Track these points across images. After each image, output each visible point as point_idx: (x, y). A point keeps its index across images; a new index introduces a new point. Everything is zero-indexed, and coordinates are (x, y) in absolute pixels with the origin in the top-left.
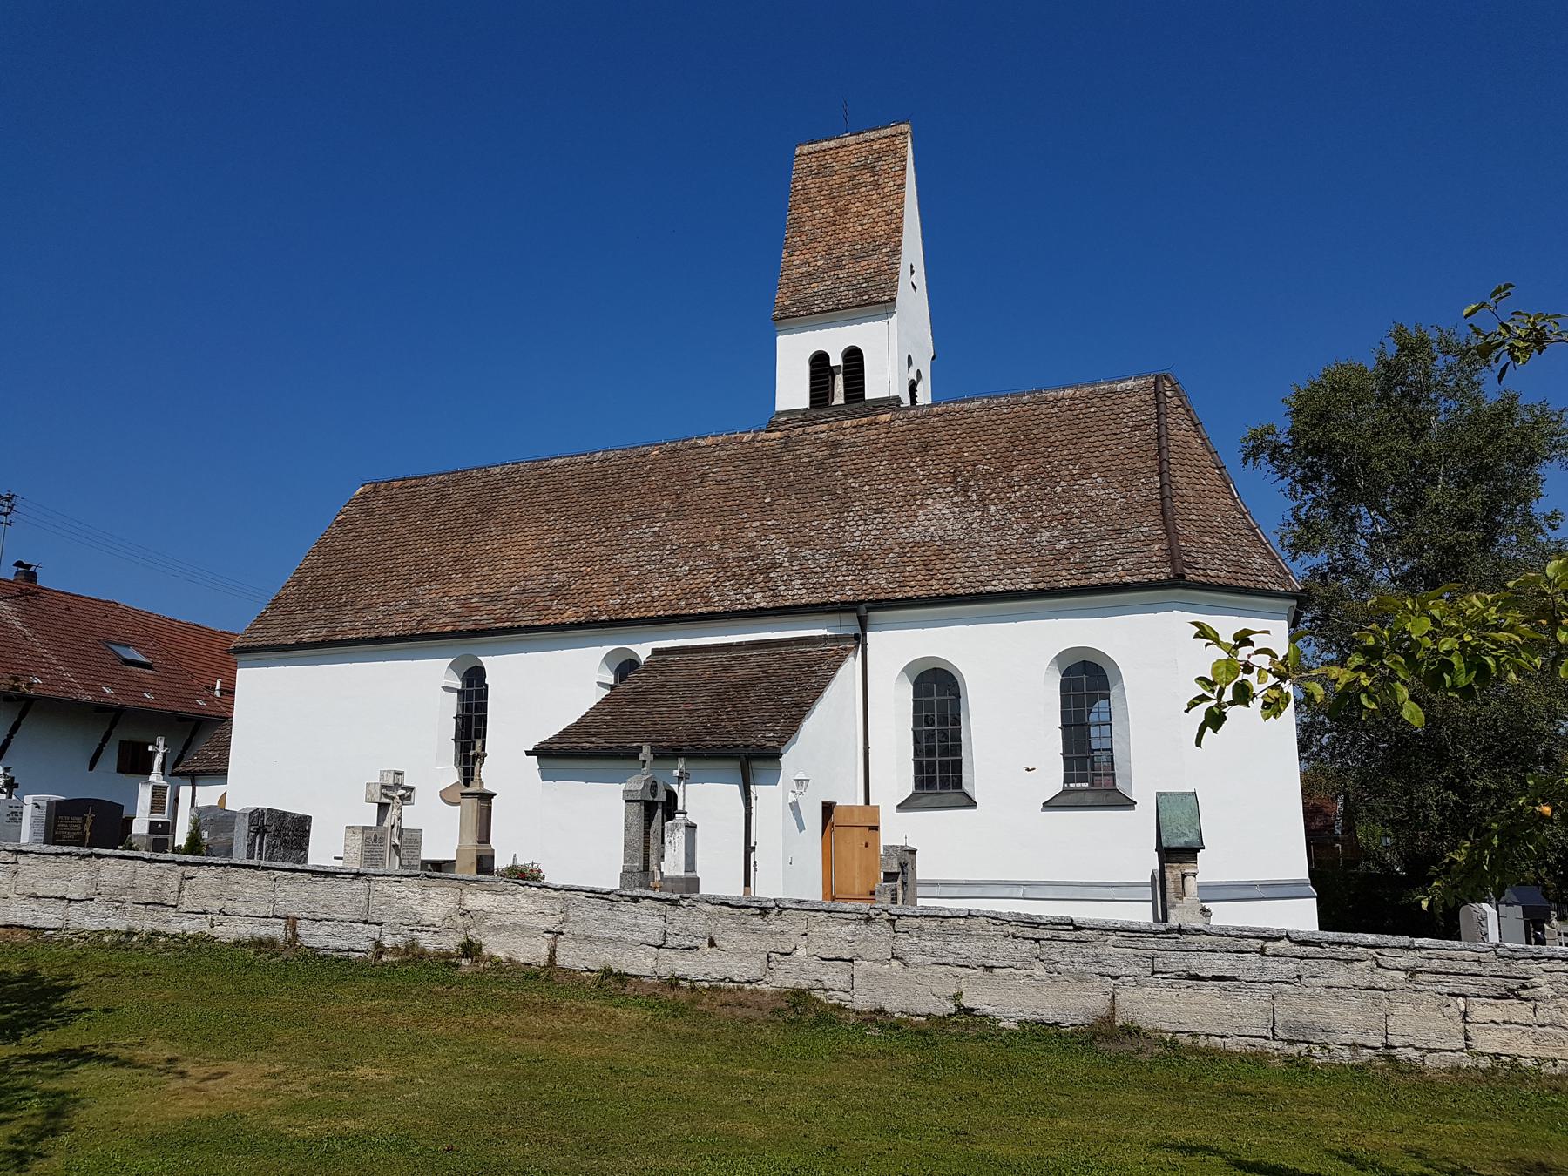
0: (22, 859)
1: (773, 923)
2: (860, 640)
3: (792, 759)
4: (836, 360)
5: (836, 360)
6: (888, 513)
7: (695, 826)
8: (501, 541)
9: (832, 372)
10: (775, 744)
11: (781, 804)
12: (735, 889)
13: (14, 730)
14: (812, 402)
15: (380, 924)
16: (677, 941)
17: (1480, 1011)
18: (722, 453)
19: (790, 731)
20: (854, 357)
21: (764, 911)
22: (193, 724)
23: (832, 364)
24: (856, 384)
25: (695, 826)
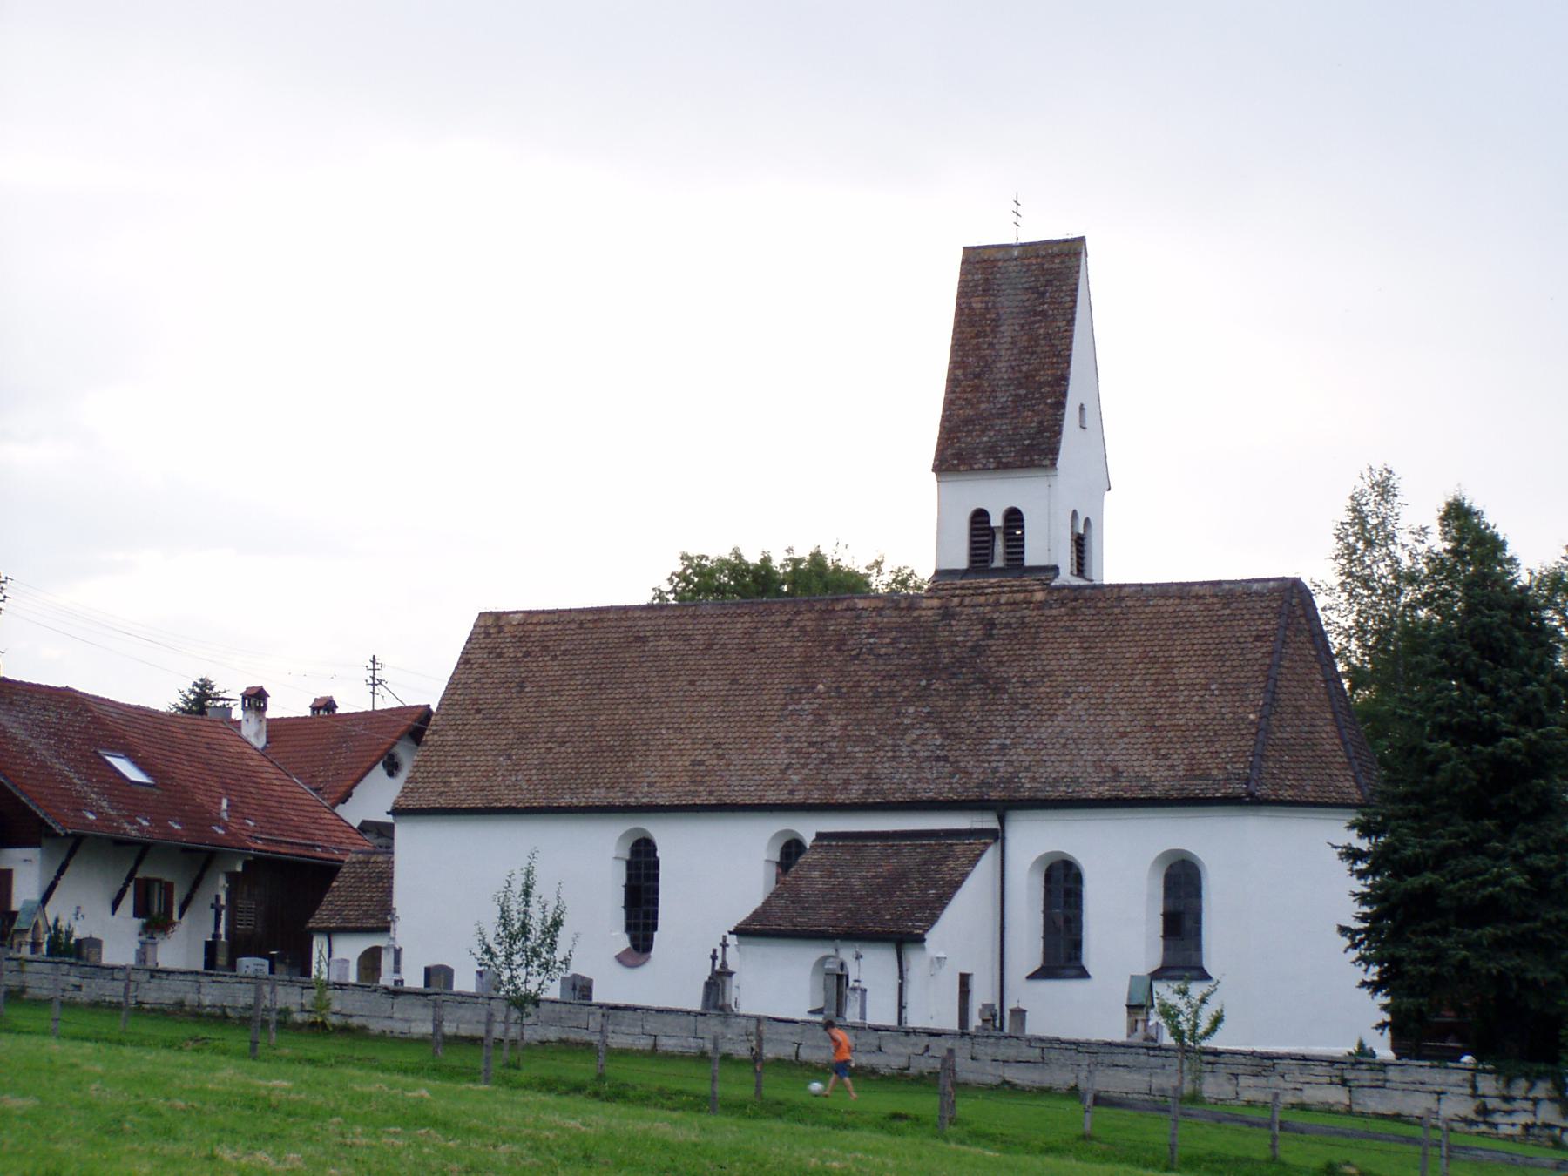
0: (492, 1002)
1: (913, 1039)
2: (997, 836)
3: (933, 937)
4: (996, 521)
5: (996, 521)
6: (1033, 710)
7: (865, 990)
8: (612, 670)
9: (992, 532)
10: (920, 932)
11: (835, 1003)
12: (892, 1021)
13: (61, 872)
14: (972, 562)
15: (702, 1038)
16: (862, 1049)
17: (1243, 1081)
18: (879, 619)
19: (932, 920)
20: (1014, 517)
21: (907, 1033)
22: (138, 849)
23: (993, 524)
24: (1015, 546)
25: (865, 990)
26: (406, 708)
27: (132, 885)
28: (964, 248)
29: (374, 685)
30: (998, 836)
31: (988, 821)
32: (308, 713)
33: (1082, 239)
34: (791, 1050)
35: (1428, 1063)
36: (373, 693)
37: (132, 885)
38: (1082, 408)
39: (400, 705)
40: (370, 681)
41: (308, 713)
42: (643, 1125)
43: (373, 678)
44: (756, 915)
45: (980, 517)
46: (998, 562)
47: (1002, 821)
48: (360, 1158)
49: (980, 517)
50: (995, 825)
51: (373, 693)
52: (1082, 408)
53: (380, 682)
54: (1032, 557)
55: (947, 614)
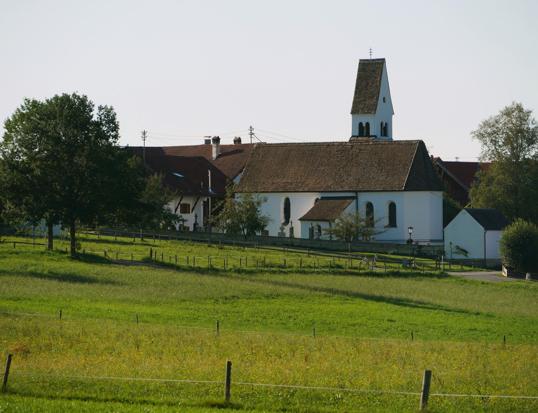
4: (364, 125)
5: (364, 125)
9: (363, 127)
17: (379, 249)
20: (368, 124)
26: (261, 143)
27: (180, 206)
28: (360, 60)
29: (251, 135)
30: (356, 198)
31: (353, 194)
32: (232, 143)
33: (384, 59)
34: (300, 244)
35: (282, 249)
36: (251, 137)
37: (180, 206)
38: (384, 98)
39: (260, 142)
40: (250, 134)
41: (232, 143)
42: (407, 271)
43: (251, 133)
44: (303, 217)
45: (361, 124)
46: (365, 134)
47: (357, 194)
48: (413, 323)
49: (361, 124)
50: (356, 195)
51: (251, 137)
52: (384, 98)
53: (253, 134)
54: (371, 133)
55: (352, 147)
